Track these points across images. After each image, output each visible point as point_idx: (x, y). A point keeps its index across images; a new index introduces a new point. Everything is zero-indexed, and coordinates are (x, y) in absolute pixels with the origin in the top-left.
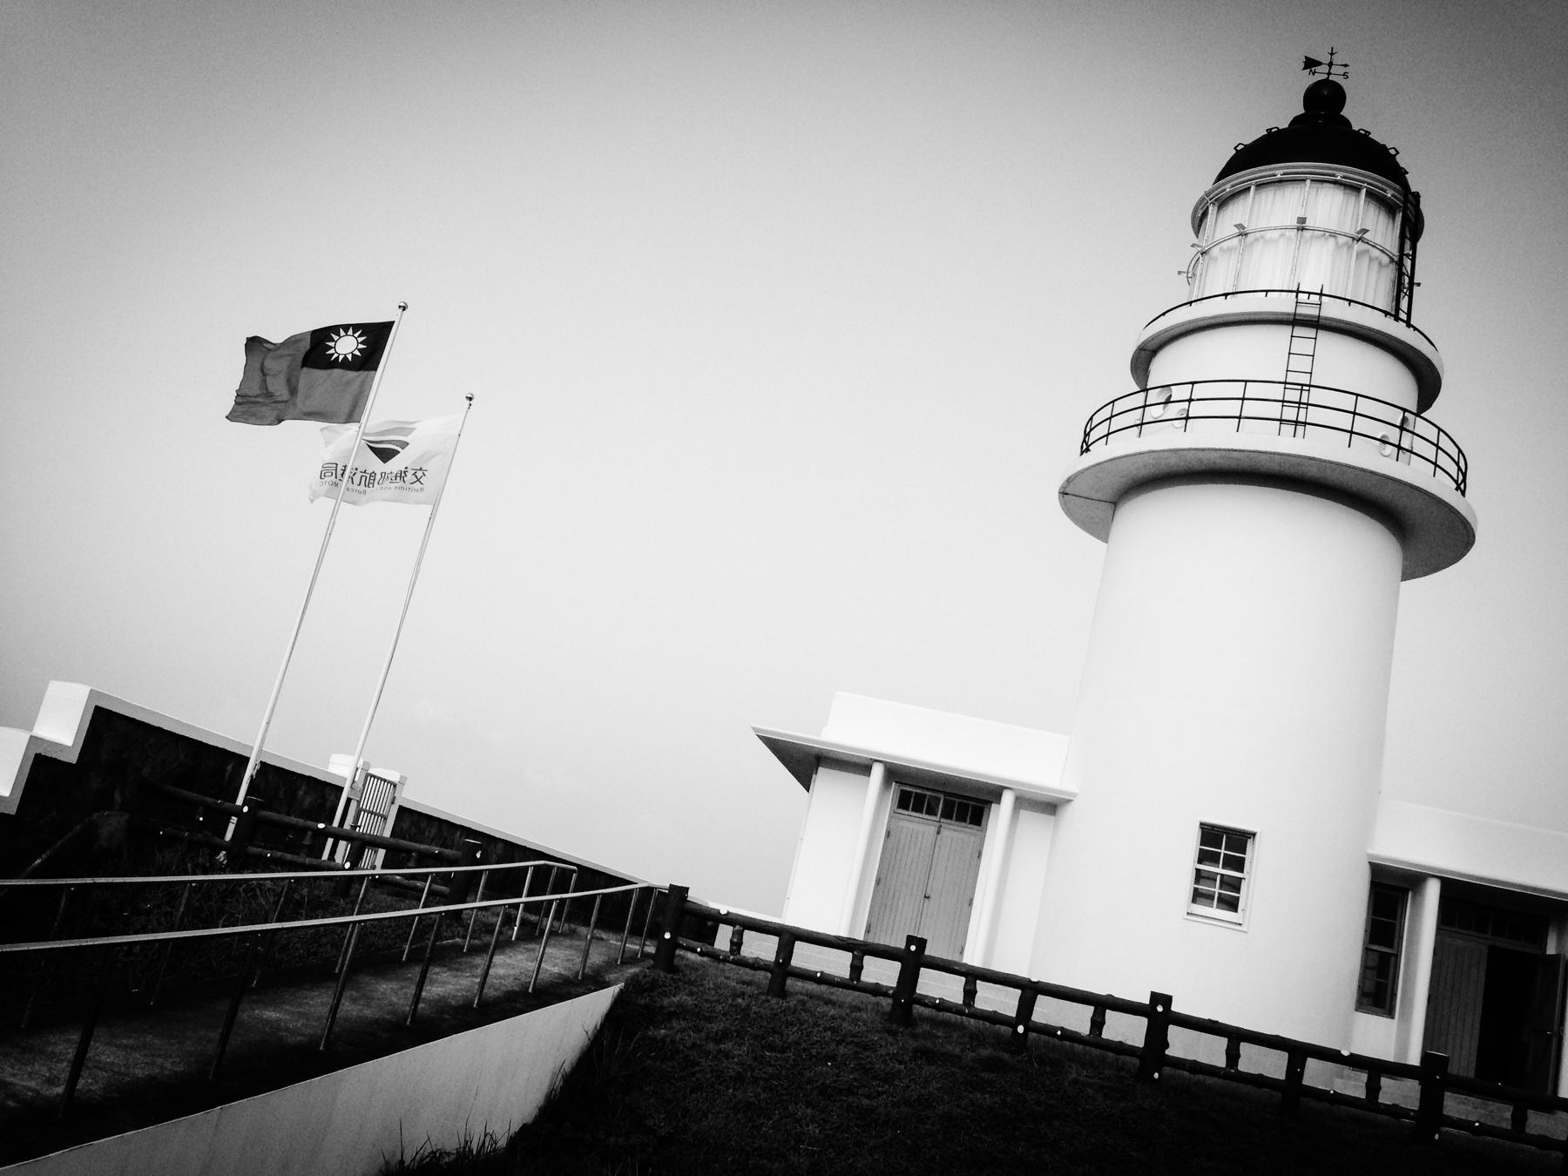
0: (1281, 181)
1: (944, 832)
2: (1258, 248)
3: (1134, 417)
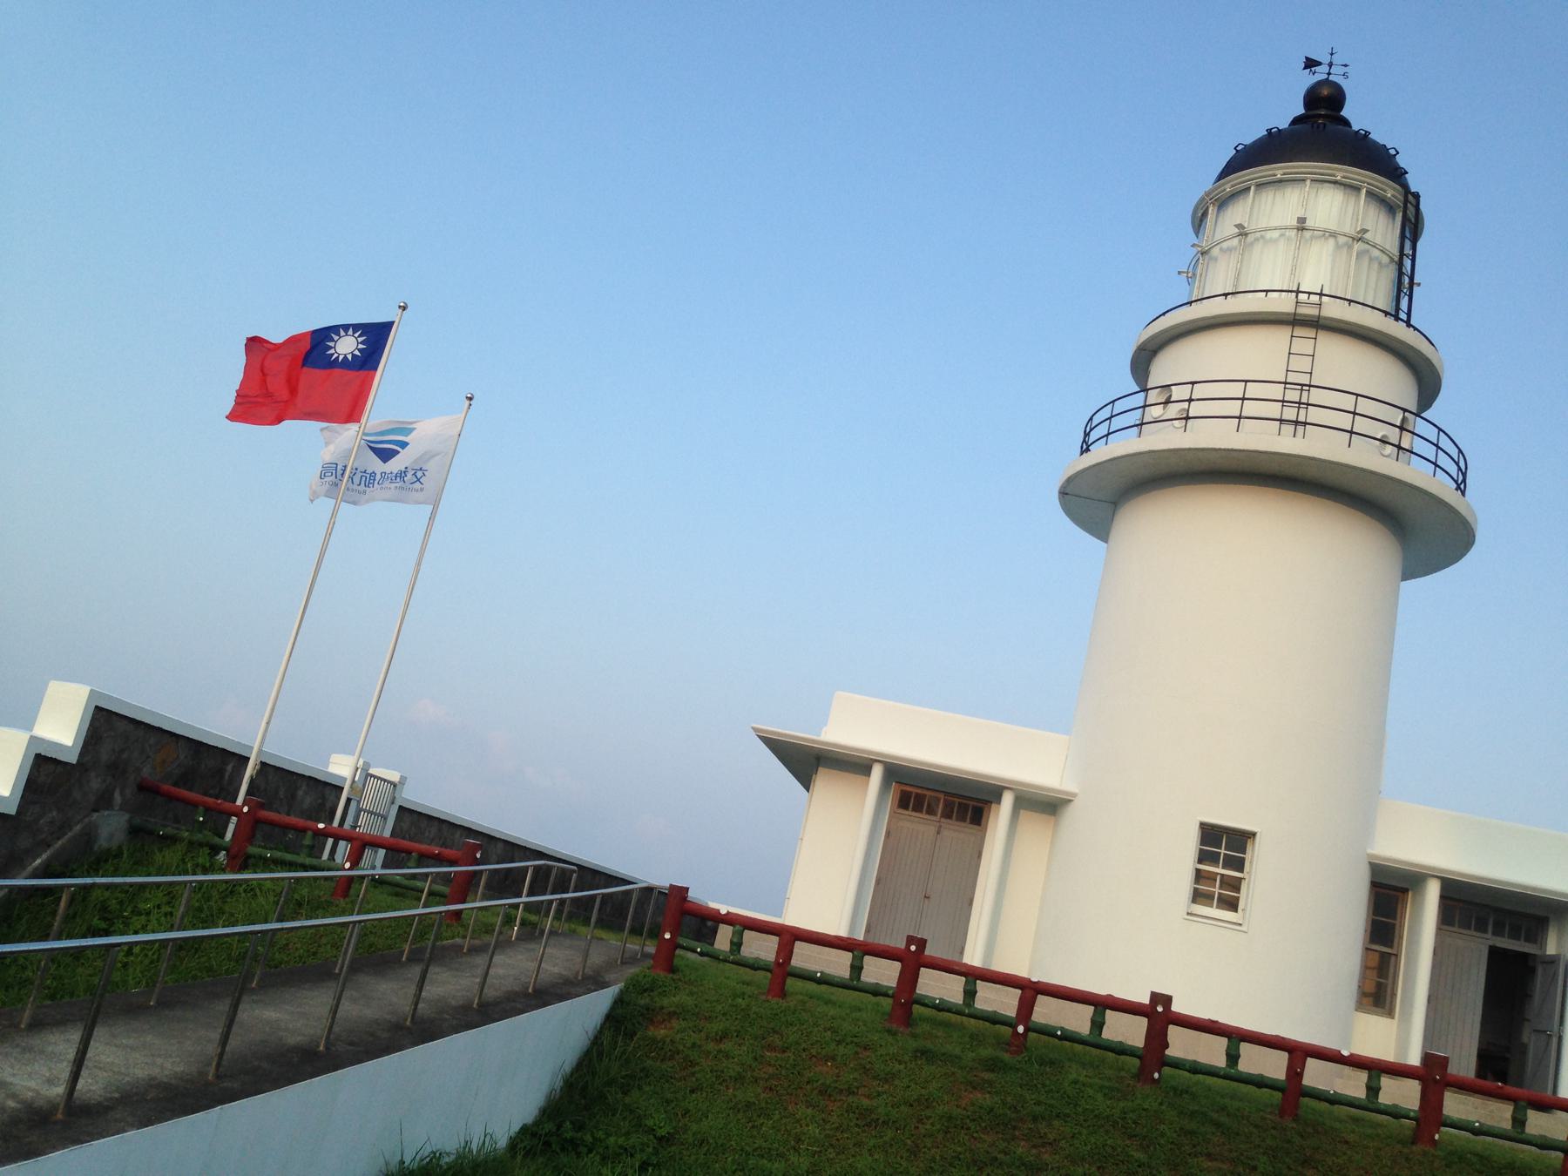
0: (1281, 181)
1: (945, 833)
2: (1258, 247)
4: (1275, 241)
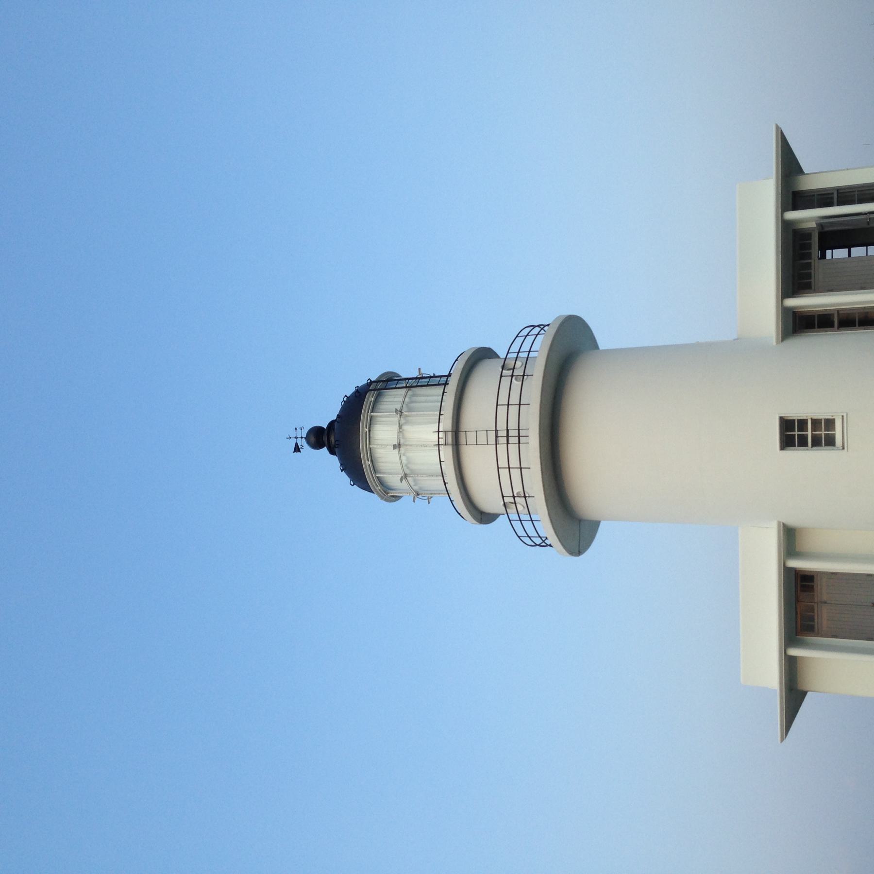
0: (372, 461)
1: (825, 597)
2: (413, 467)
3: (528, 525)
4: (408, 459)
